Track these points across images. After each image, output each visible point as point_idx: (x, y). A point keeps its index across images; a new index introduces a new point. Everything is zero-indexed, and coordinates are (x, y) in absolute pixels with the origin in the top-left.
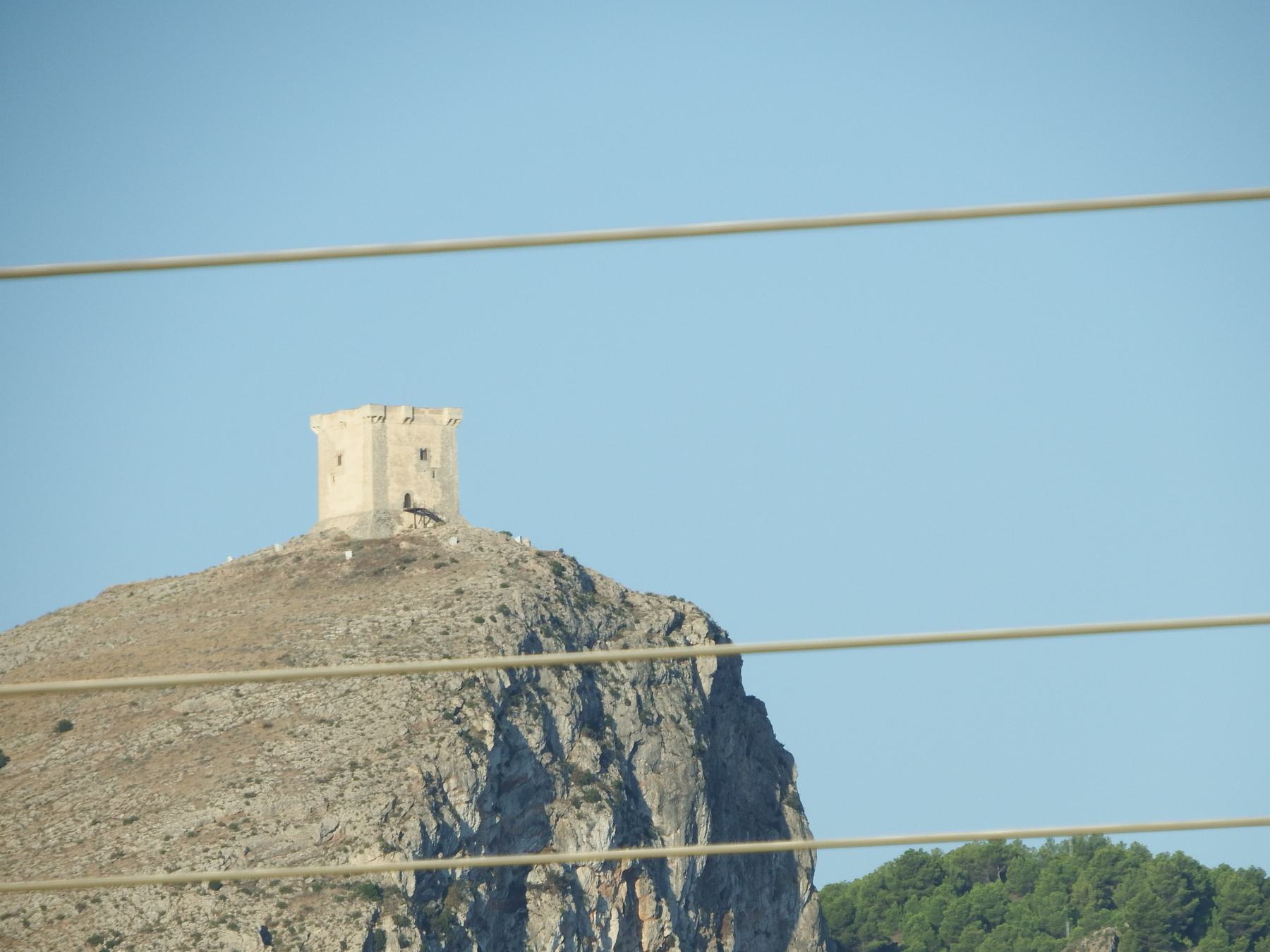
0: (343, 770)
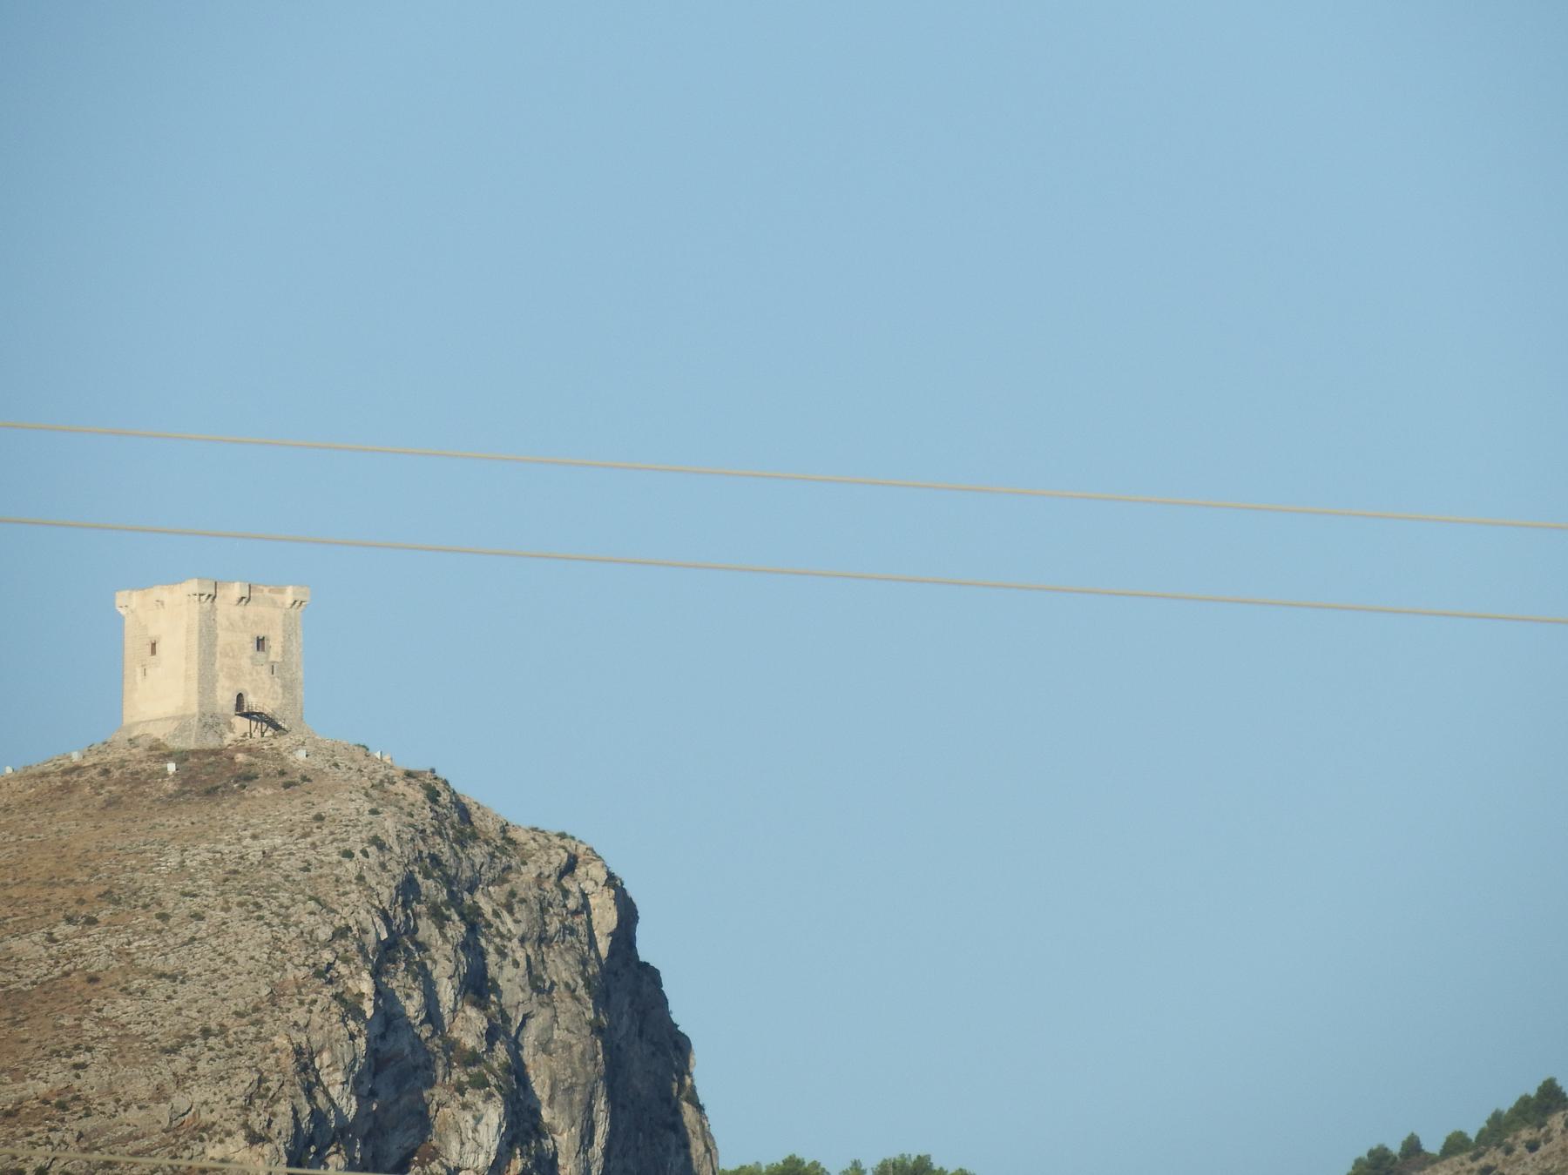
0: (194, 1038)
